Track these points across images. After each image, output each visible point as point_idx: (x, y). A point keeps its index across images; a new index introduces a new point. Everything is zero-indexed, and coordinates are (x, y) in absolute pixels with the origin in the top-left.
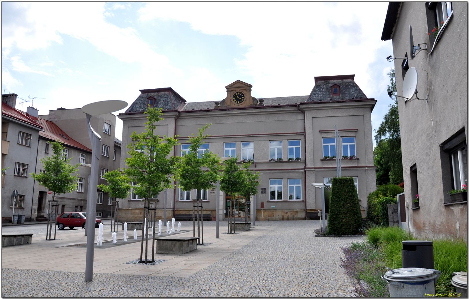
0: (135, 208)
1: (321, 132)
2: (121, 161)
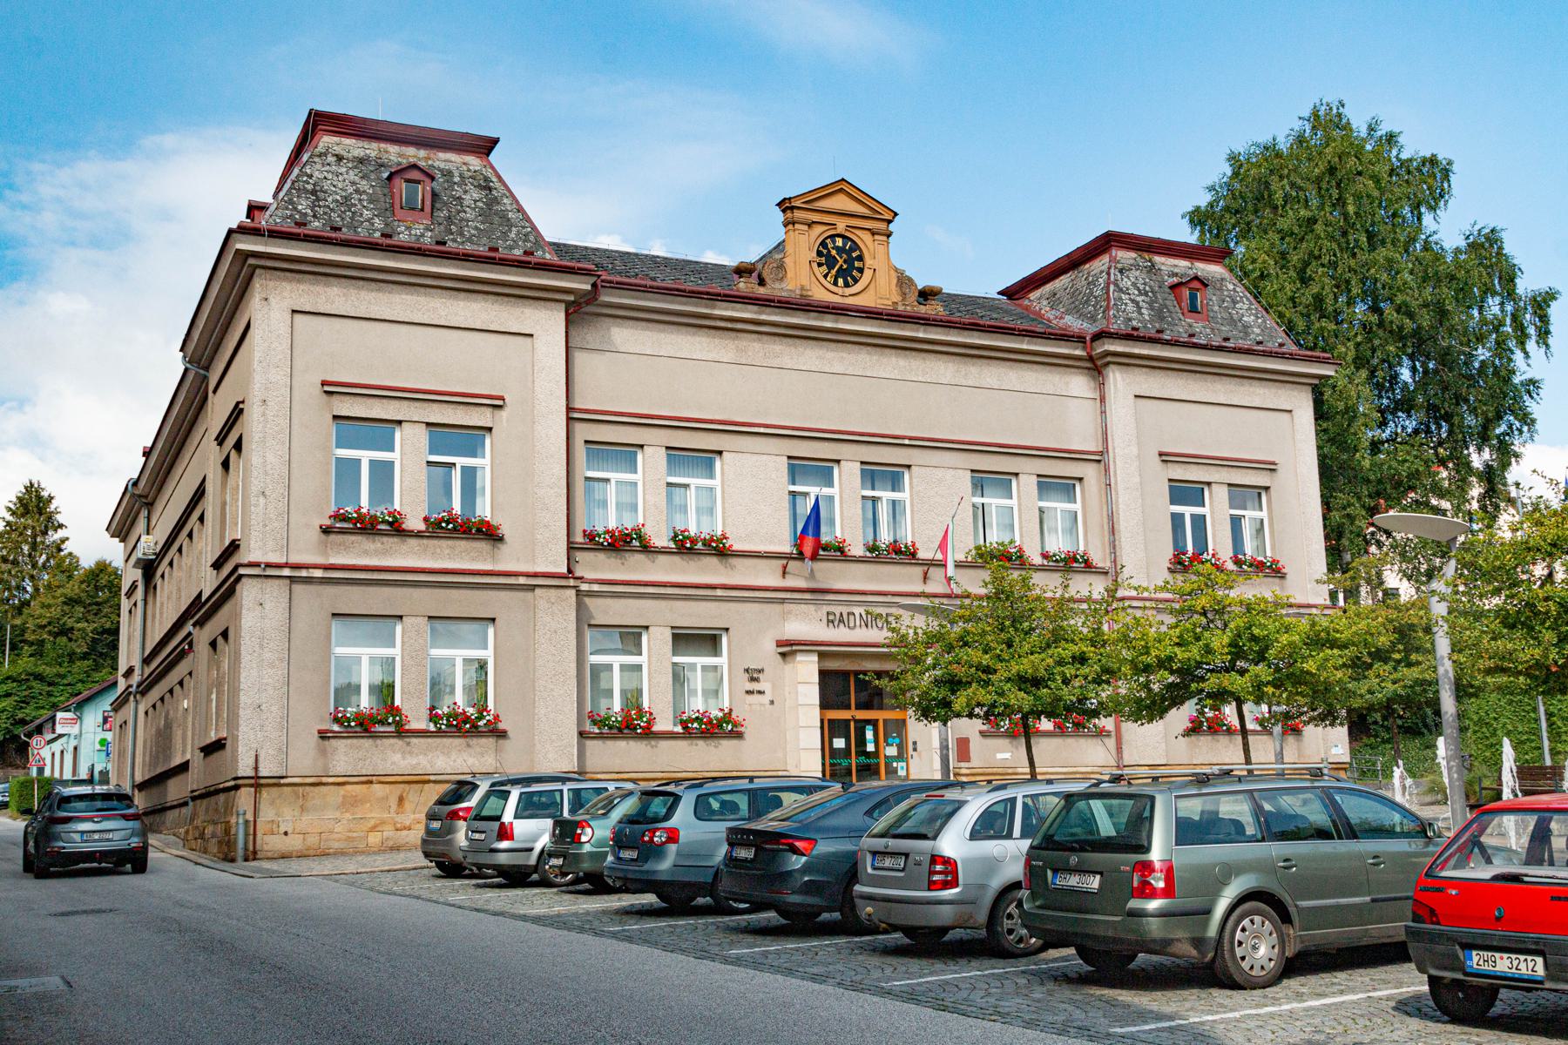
0: (364, 773)
1: (331, 389)
2: (256, 506)
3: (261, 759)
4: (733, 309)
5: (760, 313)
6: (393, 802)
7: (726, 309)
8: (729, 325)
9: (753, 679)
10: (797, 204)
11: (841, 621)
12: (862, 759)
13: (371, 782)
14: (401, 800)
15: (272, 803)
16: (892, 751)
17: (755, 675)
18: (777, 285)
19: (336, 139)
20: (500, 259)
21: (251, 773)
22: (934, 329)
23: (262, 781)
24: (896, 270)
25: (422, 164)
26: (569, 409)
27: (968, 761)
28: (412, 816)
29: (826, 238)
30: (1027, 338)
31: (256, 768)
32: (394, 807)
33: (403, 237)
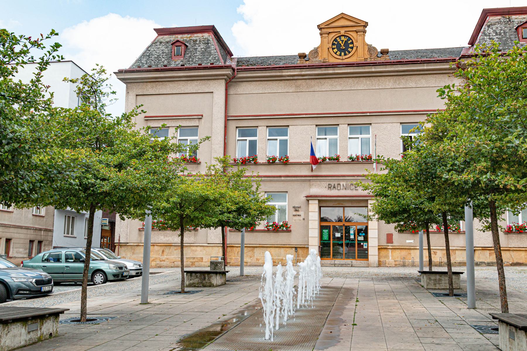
3: (121, 237)
4: (290, 72)
5: (301, 72)
6: (161, 252)
7: (287, 72)
8: (292, 78)
9: (296, 210)
10: (323, 27)
11: (334, 187)
12: (348, 241)
13: (154, 245)
14: (163, 251)
15: (125, 251)
16: (361, 238)
17: (297, 209)
18: (314, 60)
19: (162, 37)
20: (185, 68)
21: (118, 242)
22: (379, 67)
23: (121, 244)
24: (368, 45)
25: (181, 40)
26: (226, 116)
27: (392, 243)
28: (165, 257)
29: (337, 37)
30: (426, 64)
31: (119, 240)
32: (161, 254)
33: (173, 66)
